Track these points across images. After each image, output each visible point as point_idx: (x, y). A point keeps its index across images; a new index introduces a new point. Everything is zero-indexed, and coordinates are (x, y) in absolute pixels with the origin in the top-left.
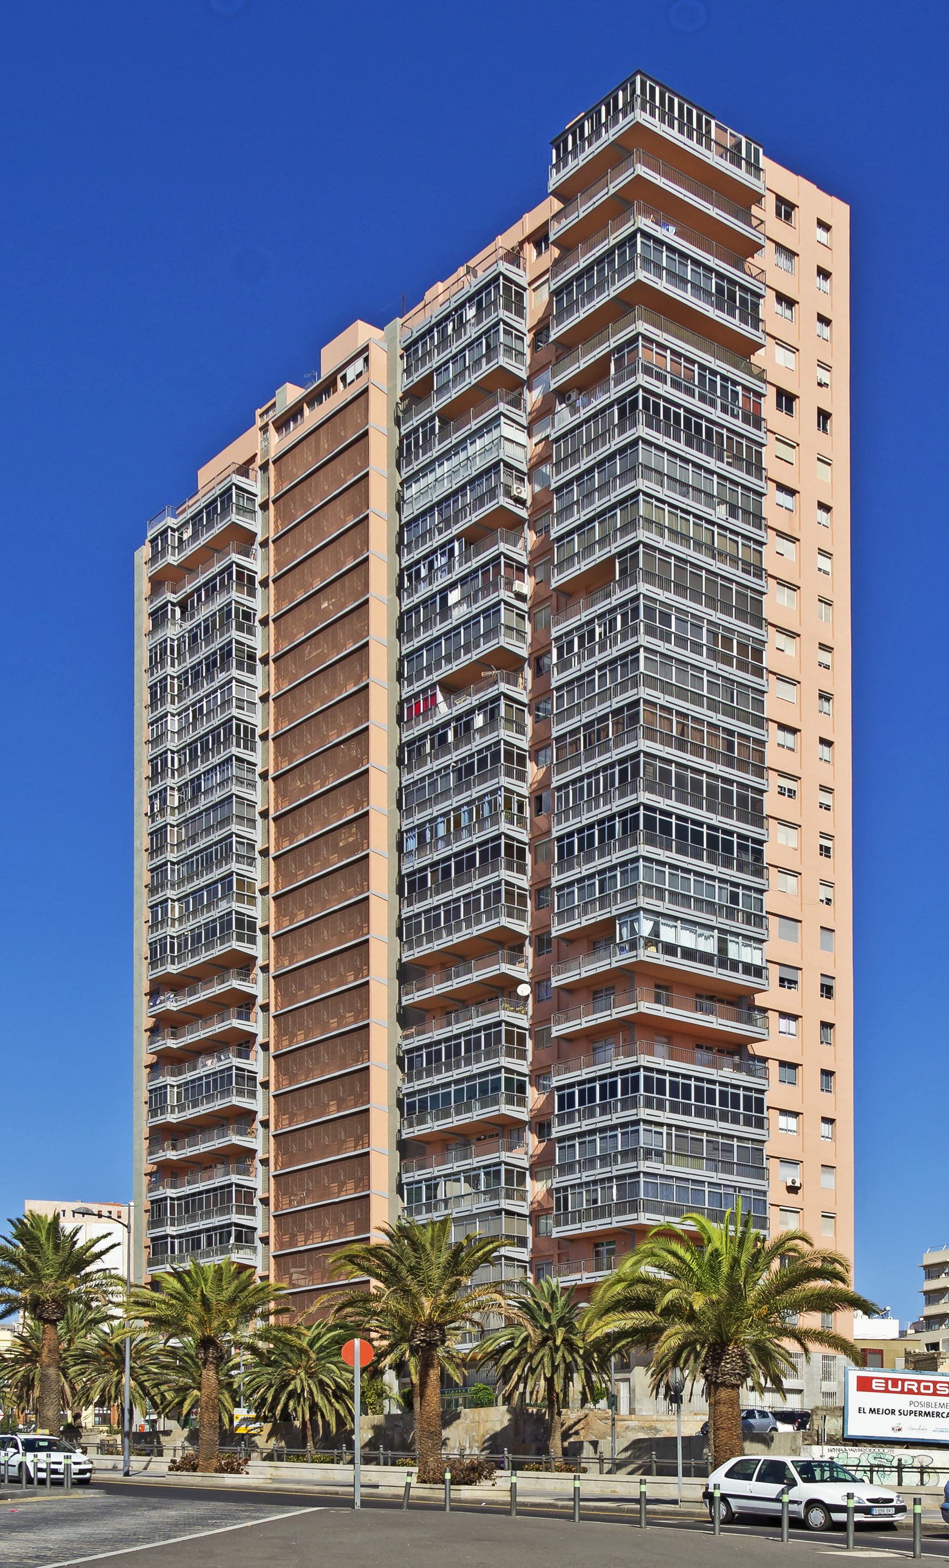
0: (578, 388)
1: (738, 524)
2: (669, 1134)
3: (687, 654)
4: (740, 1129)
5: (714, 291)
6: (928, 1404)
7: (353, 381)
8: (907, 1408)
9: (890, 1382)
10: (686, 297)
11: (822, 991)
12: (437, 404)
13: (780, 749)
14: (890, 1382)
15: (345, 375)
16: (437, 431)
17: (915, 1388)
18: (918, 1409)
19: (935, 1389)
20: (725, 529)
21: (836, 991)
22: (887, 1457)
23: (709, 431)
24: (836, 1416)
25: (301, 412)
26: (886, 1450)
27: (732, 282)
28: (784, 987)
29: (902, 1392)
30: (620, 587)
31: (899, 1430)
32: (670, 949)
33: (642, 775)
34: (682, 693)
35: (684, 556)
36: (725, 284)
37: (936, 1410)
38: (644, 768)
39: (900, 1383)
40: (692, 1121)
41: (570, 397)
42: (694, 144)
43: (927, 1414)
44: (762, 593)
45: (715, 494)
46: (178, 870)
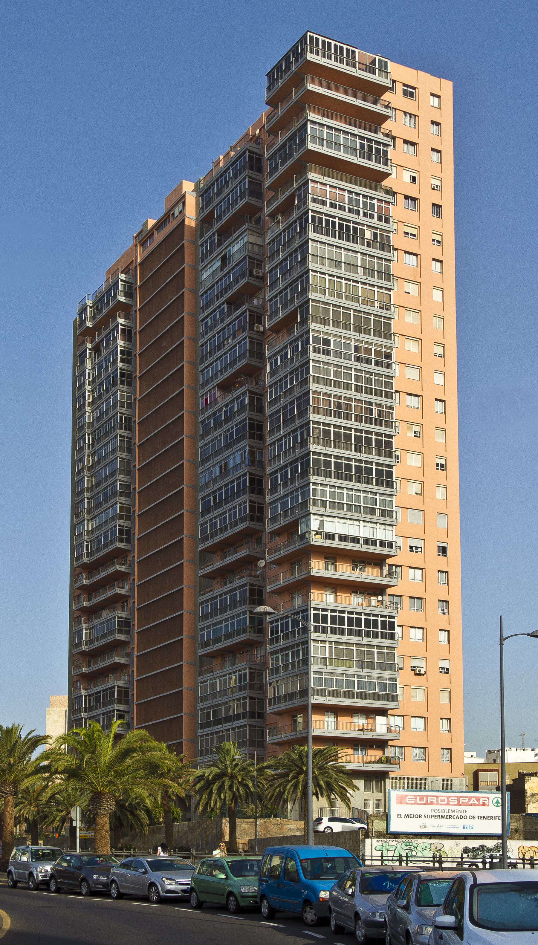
0: (281, 213)
1: (375, 280)
2: (331, 648)
3: (342, 361)
4: (380, 641)
5: (358, 148)
6: (444, 811)
7: (177, 216)
8: (430, 813)
9: (418, 798)
10: (341, 154)
11: (439, 551)
12: (217, 226)
13: (409, 409)
14: (418, 798)
15: (174, 213)
16: (216, 242)
17: (434, 801)
18: (437, 814)
19: (448, 801)
20: (366, 284)
21: (449, 552)
22: (414, 845)
23: (355, 229)
24: (383, 820)
25: (153, 234)
26: (413, 840)
27: (369, 140)
28: (413, 551)
29: (426, 803)
30: (300, 325)
31: (425, 827)
32: (330, 536)
33: (311, 435)
34: (337, 384)
35: (338, 304)
36: (365, 142)
37: (449, 814)
38: (313, 430)
39: (425, 798)
40: (347, 638)
41: (277, 218)
42: (344, 66)
43: (439, 816)
44: (390, 319)
45: (359, 264)
46: (91, 502)
